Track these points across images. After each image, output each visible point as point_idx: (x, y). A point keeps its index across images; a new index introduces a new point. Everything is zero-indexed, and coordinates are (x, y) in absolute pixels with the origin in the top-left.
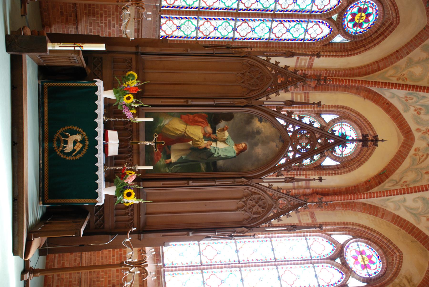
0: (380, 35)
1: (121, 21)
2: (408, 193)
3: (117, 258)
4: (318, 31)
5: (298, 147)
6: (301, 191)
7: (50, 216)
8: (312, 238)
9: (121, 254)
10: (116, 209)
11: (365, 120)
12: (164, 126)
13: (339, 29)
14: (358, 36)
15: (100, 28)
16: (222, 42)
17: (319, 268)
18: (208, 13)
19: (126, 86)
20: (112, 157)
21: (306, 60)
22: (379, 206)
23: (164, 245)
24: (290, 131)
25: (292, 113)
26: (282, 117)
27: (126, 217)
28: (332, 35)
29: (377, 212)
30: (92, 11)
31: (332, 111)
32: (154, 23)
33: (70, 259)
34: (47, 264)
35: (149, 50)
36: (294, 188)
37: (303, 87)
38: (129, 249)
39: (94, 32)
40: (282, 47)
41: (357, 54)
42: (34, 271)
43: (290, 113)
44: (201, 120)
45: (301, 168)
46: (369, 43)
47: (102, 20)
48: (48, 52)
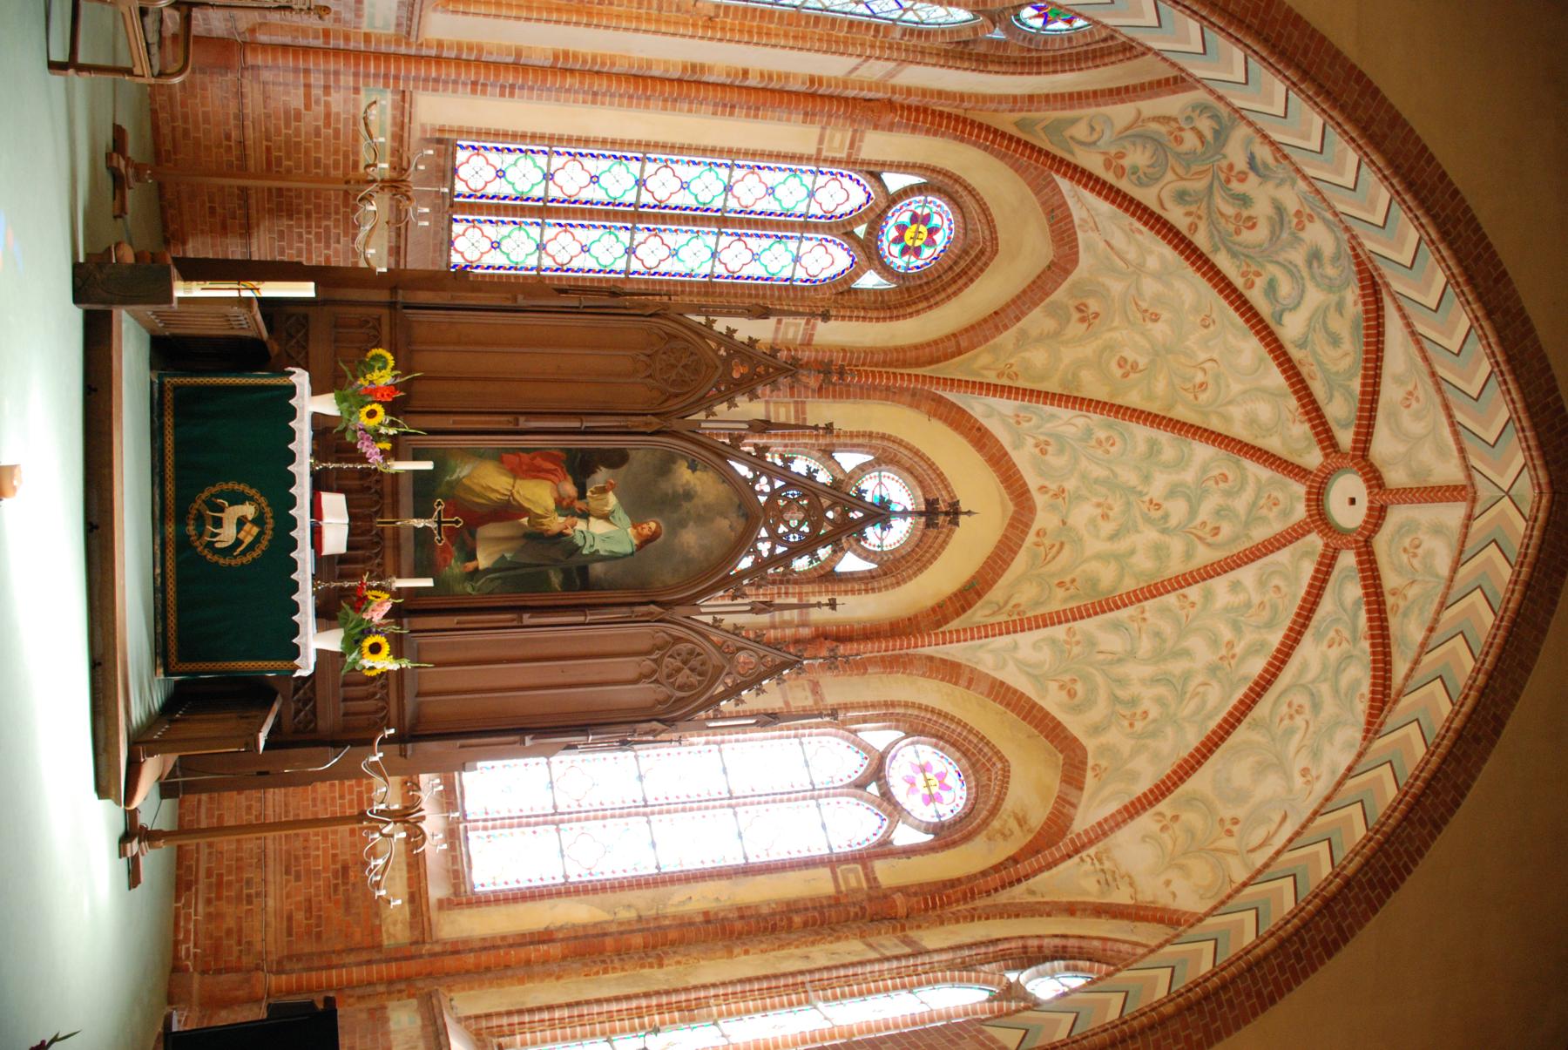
0: (959, 276)
1: (357, 227)
2: (1023, 630)
3: (351, 801)
4: (825, 260)
5: (782, 529)
6: (789, 632)
7: (183, 702)
8: (814, 739)
9: (360, 793)
10: (345, 684)
11: (932, 465)
12: (459, 480)
13: (869, 259)
14: (913, 276)
15: (304, 245)
16: (600, 280)
17: (830, 806)
18: (567, 213)
19: (366, 384)
20: (331, 557)
21: (797, 325)
22: (963, 662)
23: (463, 768)
24: (762, 493)
25: (766, 448)
26: (744, 459)
27: (370, 705)
28: (855, 271)
29: (958, 676)
30: (285, 205)
31: (859, 445)
32: (436, 233)
33: (236, 806)
34: (181, 818)
35: (424, 297)
36: (773, 626)
37: (792, 388)
38: (378, 780)
39: (290, 255)
40: (743, 295)
41: (911, 315)
42: (150, 836)
43: (762, 450)
44: (550, 466)
45: (790, 578)
46: (937, 292)
47: (309, 226)
48: (175, 304)
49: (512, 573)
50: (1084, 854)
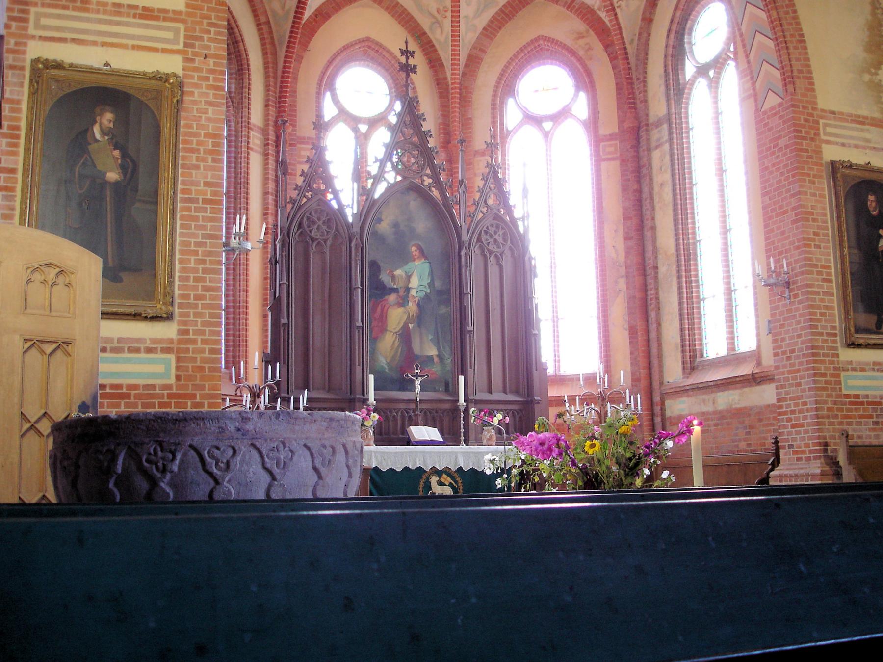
2: (459, 11)
12: (388, 364)
41: (247, 55)
49: (440, 335)
50: (616, 5)
